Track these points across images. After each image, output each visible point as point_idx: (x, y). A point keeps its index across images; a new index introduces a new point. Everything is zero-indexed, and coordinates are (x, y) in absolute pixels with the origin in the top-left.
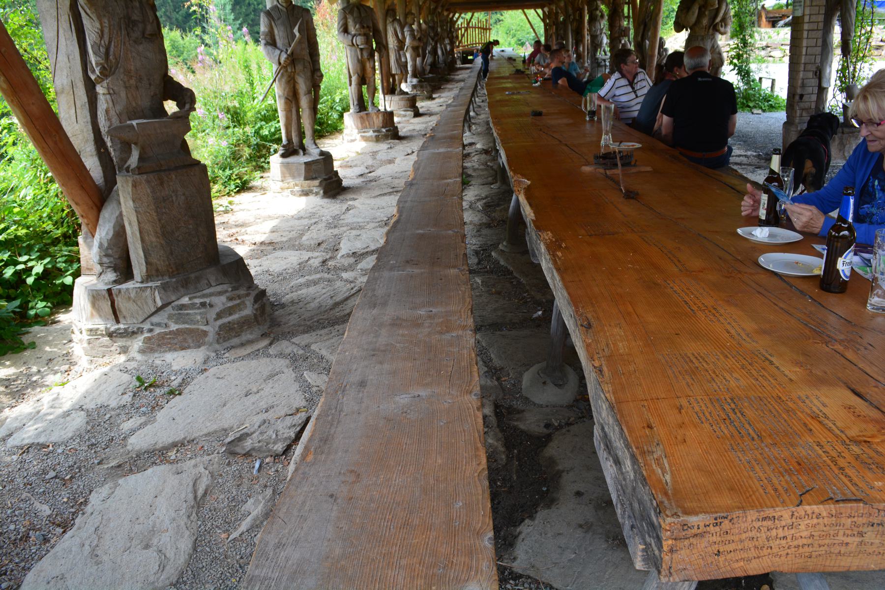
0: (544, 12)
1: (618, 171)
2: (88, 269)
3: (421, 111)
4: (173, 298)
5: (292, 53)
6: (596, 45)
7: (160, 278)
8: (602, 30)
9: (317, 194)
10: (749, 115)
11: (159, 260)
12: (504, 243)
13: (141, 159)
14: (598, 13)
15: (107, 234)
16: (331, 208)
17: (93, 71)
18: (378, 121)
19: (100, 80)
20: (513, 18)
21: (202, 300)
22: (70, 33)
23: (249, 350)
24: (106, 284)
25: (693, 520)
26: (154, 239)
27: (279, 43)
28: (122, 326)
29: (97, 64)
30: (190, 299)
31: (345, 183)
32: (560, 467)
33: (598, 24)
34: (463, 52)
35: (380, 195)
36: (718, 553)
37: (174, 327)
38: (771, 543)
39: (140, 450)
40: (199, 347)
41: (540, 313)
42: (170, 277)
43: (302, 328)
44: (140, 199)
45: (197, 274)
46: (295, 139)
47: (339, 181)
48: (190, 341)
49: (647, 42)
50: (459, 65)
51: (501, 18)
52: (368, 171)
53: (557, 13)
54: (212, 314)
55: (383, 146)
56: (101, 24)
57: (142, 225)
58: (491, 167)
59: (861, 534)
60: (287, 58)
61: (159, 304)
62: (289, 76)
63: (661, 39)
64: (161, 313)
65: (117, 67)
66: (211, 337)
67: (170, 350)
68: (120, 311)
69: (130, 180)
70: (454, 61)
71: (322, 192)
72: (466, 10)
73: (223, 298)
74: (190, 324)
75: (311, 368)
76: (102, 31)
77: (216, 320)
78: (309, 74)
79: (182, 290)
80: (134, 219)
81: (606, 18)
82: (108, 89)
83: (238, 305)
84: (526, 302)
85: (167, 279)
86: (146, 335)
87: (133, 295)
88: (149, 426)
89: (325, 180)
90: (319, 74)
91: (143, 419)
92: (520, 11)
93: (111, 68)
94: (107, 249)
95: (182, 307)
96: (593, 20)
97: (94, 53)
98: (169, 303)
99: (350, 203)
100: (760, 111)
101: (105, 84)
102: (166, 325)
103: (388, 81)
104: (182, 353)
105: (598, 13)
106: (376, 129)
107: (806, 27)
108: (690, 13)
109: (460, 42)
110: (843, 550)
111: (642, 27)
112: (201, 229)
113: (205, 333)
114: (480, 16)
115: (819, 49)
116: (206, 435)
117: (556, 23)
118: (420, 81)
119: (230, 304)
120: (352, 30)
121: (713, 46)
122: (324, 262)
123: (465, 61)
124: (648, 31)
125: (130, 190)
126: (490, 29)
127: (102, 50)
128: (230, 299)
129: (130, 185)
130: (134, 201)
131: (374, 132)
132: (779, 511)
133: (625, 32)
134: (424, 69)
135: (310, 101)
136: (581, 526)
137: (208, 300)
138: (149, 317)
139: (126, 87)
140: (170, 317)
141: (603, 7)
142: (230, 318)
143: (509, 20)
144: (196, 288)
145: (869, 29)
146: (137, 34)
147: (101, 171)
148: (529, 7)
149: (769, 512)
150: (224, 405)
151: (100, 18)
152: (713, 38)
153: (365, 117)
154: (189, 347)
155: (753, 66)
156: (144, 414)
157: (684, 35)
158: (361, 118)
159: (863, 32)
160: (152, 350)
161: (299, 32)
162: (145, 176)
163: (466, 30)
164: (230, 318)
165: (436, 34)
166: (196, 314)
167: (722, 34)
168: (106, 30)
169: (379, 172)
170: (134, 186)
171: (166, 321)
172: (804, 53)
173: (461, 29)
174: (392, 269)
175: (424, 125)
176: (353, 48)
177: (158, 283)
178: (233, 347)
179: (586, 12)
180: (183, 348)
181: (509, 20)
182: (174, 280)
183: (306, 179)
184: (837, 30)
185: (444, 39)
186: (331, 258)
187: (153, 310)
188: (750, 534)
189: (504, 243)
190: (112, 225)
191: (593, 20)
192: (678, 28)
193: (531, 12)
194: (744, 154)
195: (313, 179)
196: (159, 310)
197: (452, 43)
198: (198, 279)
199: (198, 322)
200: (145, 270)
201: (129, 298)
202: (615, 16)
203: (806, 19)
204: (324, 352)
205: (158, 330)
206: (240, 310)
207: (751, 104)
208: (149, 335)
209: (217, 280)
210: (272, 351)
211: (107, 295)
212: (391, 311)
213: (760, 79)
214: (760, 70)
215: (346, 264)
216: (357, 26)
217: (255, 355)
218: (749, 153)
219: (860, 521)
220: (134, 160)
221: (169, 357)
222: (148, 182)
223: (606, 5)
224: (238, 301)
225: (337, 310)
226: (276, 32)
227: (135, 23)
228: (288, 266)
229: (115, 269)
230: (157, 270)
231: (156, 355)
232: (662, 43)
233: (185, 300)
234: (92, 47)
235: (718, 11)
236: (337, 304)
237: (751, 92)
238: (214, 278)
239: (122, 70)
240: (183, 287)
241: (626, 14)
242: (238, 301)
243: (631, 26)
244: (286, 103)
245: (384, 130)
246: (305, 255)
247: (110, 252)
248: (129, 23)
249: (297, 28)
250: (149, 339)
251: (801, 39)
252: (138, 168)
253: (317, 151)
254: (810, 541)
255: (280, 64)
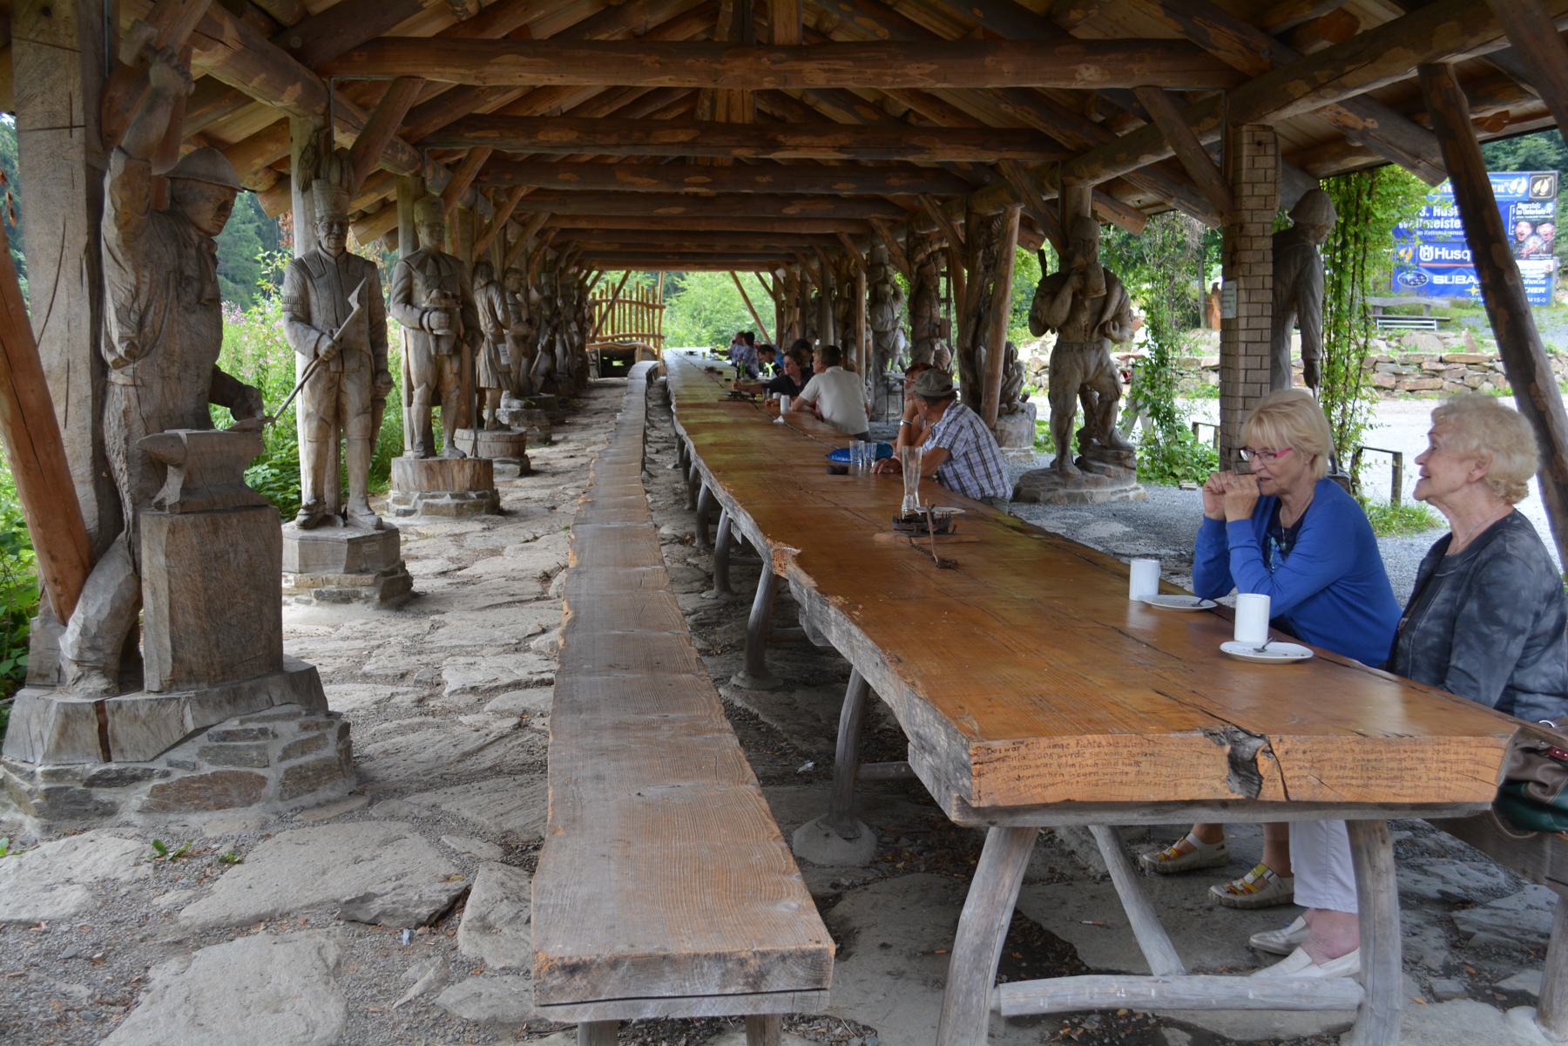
0: (776, 279)
1: (930, 539)
2: (40, 675)
3: (534, 464)
4: (213, 720)
5: (341, 339)
6: (884, 352)
7: (194, 685)
8: (896, 321)
9: (367, 600)
10: (1175, 490)
11: (195, 655)
12: (741, 675)
13: (185, 490)
14: (888, 288)
15: (99, 611)
16: (400, 628)
17: (112, 348)
18: (462, 477)
19: (120, 364)
20: (707, 288)
21: (261, 725)
22: (78, 286)
23: (334, 811)
24: (90, 695)
25: (996, 744)
26: (192, 621)
27: (318, 318)
28: (113, 766)
29: (121, 339)
30: (242, 722)
31: (417, 586)
32: (857, 924)
33: (887, 310)
34: (603, 353)
35: (490, 606)
36: (1019, 778)
37: (207, 769)
38: (1063, 771)
39: (205, 924)
40: (250, 804)
41: (810, 765)
42: (210, 685)
43: (415, 786)
44: (178, 554)
45: (253, 683)
46: (329, 497)
47: (408, 580)
48: (234, 793)
49: (983, 350)
50: (593, 378)
51: (682, 284)
52: (454, 566)
53: (803, 283)
54: (275, 750)
55: (473, 527)
56: (137, 278)
57: (175, 596)
58: (696, 566)
59: (1137, 763)
60: (332, 347)
61: (190, 727)
62: (331, 380)
63: (1009, 345)
64: (188, 744)
65: (153, 346)
66: (271, 788)
67: (197, 809)
68: (115, 740)
69: (166, 522)
70: (584, 371)
71: (377, 596)
72: (617, 266)
73: (293, 726)
74: (238, 765)
75: (450, 832)
76: (137, 289)
77: (281, 759)
78: (368, 377)
79: (228, 707)
80: (163, 585)
81: (905, 298)
82: (134, 378)
83: (316, 738)
84: (785, 754)
85: (204, 687)
86: (157, 782)
87: (143, 712)
88: (204, 900)
89: (385, 574)
90: (385, 379)
91: (190, 893)
92: (727, 273)
93: (143, 347)
94: (95, 636)
95: (228, 735)
96: (877, 301)
97: (120, 321)
98: (205, 729)
99: (436, 617)
100: (1194, 485)
101: (129, 370)
102: (195, 767)
103: (471, 401)
104: (219, 814)
105: (888, 288)
106: (457, 490)
107: (1242, 336)
108: (1058, 302)
109: (598, 330)
110: (1124, 779)
111: (973, 321)
112: (266, 610)
113: (262, 781)
114: (639, 279)
115: (1267, 374)
116: (308, 907)
117: (802, 302)
118: (527, 406)
119: (304, 736)
120: (423, 299)
121: (1100, 363)
122: (421, 701)
123: (606, 370)
124: (985, 329)
125: (164, 538)
126: (662, 308)
127: (134, 317)
128: (305, 728)
129: (165, 529)
130: (167, 556)
131: (453, 497)
132: (1066, 740)
133: (941, 329)
134: (531, 383)
135: (366, 428)
136: (889, 973)
137: (269, 726)
138: (167, 750)
139: (163, 378)
140: (203, 753)
141: (898, 278)
142: (302, 760)
143: (700, 290)
144: (249, 706)
145: (1362, 341)
146: (189, 297)
147: (96, 509)
148: (745, 267)
149: (1058, 740)
150: (324, 873)
151: (136, 269)
152: (1100, 347)
153: (437, 468)
154: (231, 805)
155: (1179, 402)
156: (187, 887)
157: (1051, 339)
158: (429, 468)
159: (1353, 347)
160: (165, 808)
161: (359, 300)
162: (192, 518)
163: (611, 307)
164: (302, 760)
165: (556, 312)
166: (250, 747)
167: (1115, 341)
168: (145, 288)
169: (479, 568)
170: (172, 531)
171: (195, 759)
172: (1242, 379)
173: (599, 303)
174: (590, 673)
175: (548, 492)
176: (421, 334)
177: (192, 694)
178: (303, 809)
179: (864, 284)
180: (220, 806)
181: (700, 290)
182: (217, 690)
183: (348, 570)
184: (1296, 340)
185: (568, 323)
186: (431, 695)
187: (177, 738)
188: (1044, 761)
189: (741, 675)
190: (109, 597)
191: (877, 301)
192: (1038, 328)
193: (748, 278)
194: (1152, 552)
195: (362, 572)
196: (188, 737)
197: (582, 332)
198: (254, 691)
199: (252, 760)
200: (169, 671)
201: (136, 717)
202: (921, 296)
203: (1243, 323)
204: (466, 813)
205: (178, 774)
206: (318, 748)
207: (1178, 472)
208: (163, 782)
209: (283, 695)
210: (373, 812)
211: (93, 713)
212: (606, 717)
213: (1195, 425)
214: (1191, 410)
215: (462, 704)
216: (434, 293)
217: (349, 816)
218: (1163, 552)
219: (1136, 750)
220: (172, 490)
221: (195, 820)
222: (195, 526)
223: (905, 276)
224: (316, 733)
225: (469, 763)
226: (313, 298)
227: (188, 280)
228: (357, 705)
229: (104, 672)
230: (190, 672)
231: (172, 817)
232: (1011, 355)
233: (233, 724)
234: (117, 311)
235: (1106, 301)
236: (467, 755)
237: (1176, 448)
238: (279, 692)
239: (161, 351)
240: (229, 702)
241: (943, 295)
242: (316, 733)
243: (953, 316)
244: (320, 428)
245: (473, 495)
246: (385, 691)
247: (100, 642)
248: (182, 280)
249: (355, 294)
250: (162, 788)
251: (1236, 356)
252: (182, 504)
253: (371, 520)
254: (1093, 770)
255: (316, 355)
